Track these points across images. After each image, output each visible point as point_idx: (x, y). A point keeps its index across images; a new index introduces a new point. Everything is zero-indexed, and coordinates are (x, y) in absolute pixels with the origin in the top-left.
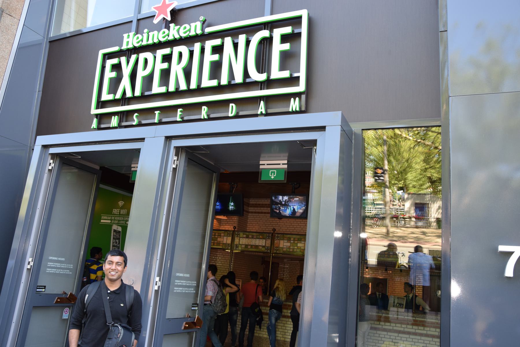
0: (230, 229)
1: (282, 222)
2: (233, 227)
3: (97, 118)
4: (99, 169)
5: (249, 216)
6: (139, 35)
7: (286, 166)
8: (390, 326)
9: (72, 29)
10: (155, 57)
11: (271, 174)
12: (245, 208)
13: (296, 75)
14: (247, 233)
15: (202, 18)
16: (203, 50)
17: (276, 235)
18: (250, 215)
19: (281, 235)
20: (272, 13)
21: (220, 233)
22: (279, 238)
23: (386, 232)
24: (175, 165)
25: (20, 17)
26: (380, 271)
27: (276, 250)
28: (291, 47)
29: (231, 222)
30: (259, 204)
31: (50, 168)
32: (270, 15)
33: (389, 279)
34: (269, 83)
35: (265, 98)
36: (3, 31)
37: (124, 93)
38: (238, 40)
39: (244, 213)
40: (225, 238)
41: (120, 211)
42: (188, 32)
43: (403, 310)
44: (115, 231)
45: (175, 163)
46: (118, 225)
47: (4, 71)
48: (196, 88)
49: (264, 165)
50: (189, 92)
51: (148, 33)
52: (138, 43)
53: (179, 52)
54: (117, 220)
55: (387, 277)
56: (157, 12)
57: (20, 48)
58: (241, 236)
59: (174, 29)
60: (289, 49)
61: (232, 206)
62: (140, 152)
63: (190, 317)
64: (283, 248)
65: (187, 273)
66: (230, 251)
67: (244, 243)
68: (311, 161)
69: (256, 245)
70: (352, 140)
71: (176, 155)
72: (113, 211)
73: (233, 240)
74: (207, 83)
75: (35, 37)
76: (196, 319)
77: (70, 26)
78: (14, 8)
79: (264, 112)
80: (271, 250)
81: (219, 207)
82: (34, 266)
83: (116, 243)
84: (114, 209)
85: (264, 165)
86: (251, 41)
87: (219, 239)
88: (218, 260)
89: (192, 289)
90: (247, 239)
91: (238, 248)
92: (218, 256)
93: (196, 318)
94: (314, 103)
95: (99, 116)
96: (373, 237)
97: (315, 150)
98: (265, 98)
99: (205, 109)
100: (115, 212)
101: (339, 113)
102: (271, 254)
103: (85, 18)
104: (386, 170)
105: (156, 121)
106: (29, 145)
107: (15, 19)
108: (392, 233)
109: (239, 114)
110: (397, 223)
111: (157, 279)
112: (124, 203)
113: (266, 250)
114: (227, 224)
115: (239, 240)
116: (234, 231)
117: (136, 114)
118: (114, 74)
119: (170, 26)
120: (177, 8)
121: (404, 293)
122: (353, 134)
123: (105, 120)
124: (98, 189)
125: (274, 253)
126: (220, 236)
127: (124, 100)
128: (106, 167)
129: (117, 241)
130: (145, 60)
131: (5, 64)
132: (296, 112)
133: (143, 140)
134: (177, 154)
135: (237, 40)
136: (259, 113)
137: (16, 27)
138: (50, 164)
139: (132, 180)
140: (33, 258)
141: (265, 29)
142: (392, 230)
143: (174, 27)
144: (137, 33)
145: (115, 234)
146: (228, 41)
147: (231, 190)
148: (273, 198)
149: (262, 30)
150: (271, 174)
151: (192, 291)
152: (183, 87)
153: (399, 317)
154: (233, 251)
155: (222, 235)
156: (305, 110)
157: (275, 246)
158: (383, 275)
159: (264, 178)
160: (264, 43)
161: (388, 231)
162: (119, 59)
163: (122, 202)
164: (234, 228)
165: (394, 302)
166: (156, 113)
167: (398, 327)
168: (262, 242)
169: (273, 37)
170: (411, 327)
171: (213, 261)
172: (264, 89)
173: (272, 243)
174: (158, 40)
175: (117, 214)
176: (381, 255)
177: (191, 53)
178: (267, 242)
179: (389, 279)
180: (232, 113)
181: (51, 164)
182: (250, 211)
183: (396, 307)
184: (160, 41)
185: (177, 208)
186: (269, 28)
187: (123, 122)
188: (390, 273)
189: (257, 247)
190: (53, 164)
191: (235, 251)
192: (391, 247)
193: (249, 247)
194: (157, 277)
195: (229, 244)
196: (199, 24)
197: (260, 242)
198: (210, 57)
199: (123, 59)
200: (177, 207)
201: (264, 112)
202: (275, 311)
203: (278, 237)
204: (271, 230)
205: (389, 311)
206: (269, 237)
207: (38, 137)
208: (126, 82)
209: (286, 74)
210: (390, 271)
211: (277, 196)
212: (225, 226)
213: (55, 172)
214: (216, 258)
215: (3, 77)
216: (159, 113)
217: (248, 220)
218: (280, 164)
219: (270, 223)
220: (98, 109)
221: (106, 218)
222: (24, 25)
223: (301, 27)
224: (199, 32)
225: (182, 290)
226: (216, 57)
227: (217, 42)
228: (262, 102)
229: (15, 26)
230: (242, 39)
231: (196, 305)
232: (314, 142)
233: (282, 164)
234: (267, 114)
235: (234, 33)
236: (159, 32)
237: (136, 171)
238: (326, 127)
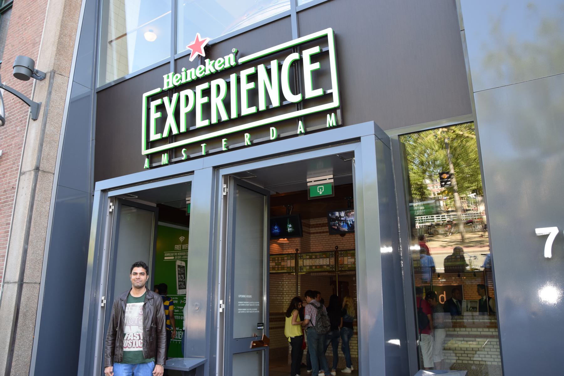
0: (293, 252)
1: (345, 239)
2: (295, 250)
3: (148, 158)
4: (156, 206)
5: (311, 238)
6: (178, 75)
7: (332, 181)
8: (466, 331)
10: (195, 93)
11: (319, 190)
12: (305, 229)
13: (329, 92)
14: (310, 254)
15: (234, 50)
17: (340, 252)
18: (312, 236)
19: (344, 251)
20: (299, 36)
21: (283, 257)
22: (342, 255)
23: (461, 239)
24: (225, 192)
25: (70, 74)
26: (453, 278)
27: (340, 267)
28: (321, 65)
29: (294, 245)
30: (320, 224)
31: (111, 210)
32: (298, 38)
33: (464, 285)
34: (305, 103)
35: (302, 118)
36: (56, 90)
37: (171, 131)
39: (303, 233)
40: (289, 261)
41: (182, 246)
42: (223, 65)
43: (477, 313)
44: (179, 266)
45: (225, 191)
46: (181, 261)
47: (60, 126)
49: (311, 182)
50: (231, 122)
51: (186, 72)
52: (178, 82)
54: (180, 256)
55: (460, 284)
56: (192, 50)
57: (71, 103)
58: (304, 258)
59: (209, 64)
61: (291, 228)
62: (191, 185)
63: (257, 336)
64: (348, 265)
65: (249, 294)
66: (295, 274)
67: (308, 265)
69: (320, 264)
70: (390, 147)
71: (225, 183)
72: (175, 247)
73: (297, 263)
74: (246, 111)
76: (263, 338)
77: (113, 74)
78: (64, 67)
79: (303, 131)
80: (336, 268)
81: (277, 230)
82: (107, 303)
83: (182, 278)
84: (176, 246)
85: (311, 182)
86: (282, 65)
87: (283, 264)
88: (285, 285)
89: (256, 309)
90: (311, 260)
91: (303, 270)
92: (285, 281)
93: (263, 337)
94: (350, 116)
95: (149, 156)
96: (449, 245)
97: (354, 161)
98: (302, 118)
99: (247, 136)
100: (177, 248)
101: (371, 124)
102: (336, 272)
103: (127, 65)
104: (452, 174)
105: (203, 153)
106: (89, 192)
107: (65, 77)
108: (468, 239)
109: (280, 136)
110: (474, 227)
111: (221, 302)
112: (184, 238)
113: (331, 269)
114: (289, 248)
115: (303, 261)
116: (296, 254)
117: (184, 149)
118: (159, 115)
119: (205, 62)
120: (210, 44)
121: (478, 296)
122: (391, 141)
123: (156, 159)
124: (157, 227)
125: (339, 271)
126: (284, 260)
127: (172, 138)
128: (162, 203)
129: (182, 276)
130: (186, 97)
131: (61, 119)
132: (333, 127)
133: (192, 173)
134: (226, 182)
135: (269, 66)
136: (298, 132)
137: (67, 84)
138: (110, 206)
139: (188, 213)
141: (294, 52)
142: (467, 236)
143: (209, 62)
144: (176, 72)
145: (180, 270)
146: (261, 68)
147: (288, 212)
148: (330, 215)
150: (319, 190)
151: (256, 311)
152: (225, 117)
153: (475, 321)
154: (298, 273)
155: (286, 258)
156: (342, 124)
157: (340, 264)
158: (457, 282)
159: (312, 195)
160: (295, 65)
161: (463, 237)
162: (162, 100)
163: (182, 238)
164: (297, 250)
165: (467, 307)
166: (202, 146)
167: (474, 331)
168: (326, 261)
169: (302, 59)
170: (487, 330)
171: (280, 287)
172: (300, 110)
173: (336, 261)
174: (195, 76)
175: (179, 249)
176: (447, 260)
177: (228, 84)
178: (331, 260)
179: (464, 285)
180: (273, 136)
181: (111, 207)
182: (311, 232)
183: (470, 311)
184: (198, 78)
185: (232, 233)
186: (298, 51)
187: (173, 159)
188: (464, 279)
189: (321, 266)
190: (113, 207)
191: (299, 274)
192: (458, 250)
193: (314, 268)
194: (221, 300)
195: (293, 267)
196: (232, 56)
197: (324, 261)
198: (246, 86)
199: (166, 99)
200: (231, 232)
201: (303, 131)
202: (346, 328)
203: (341, 254)
204: (334, 248)
205: (463, 316)
206: (332, 255)
207: (96, 183)
208: (171, 121)
209: (319, 92)
210: (463, 277)
211: (334, 212)
212: (288, 250)
213: (116, 214)
214: (282, 283)
215: (59, 132)
216: (205, 146)
217: (311, 242)
218: (326, 179)
219: (333, 242)
220: (148, 149)
221: (169, 254)
223: (328, 46)
224: (233, 63)
225: (245, 311)
226: (252, 85)
227: (251, 70)
228: (300, 122)
229: (65, 83)
230: (274, 64)
231: (262, 325)
232: (351, 154)
233: (328, 178)
234: (306, 133)
235: (265, 60)
236: (196, 68)
237: (190, 204)
238: (361, 138)
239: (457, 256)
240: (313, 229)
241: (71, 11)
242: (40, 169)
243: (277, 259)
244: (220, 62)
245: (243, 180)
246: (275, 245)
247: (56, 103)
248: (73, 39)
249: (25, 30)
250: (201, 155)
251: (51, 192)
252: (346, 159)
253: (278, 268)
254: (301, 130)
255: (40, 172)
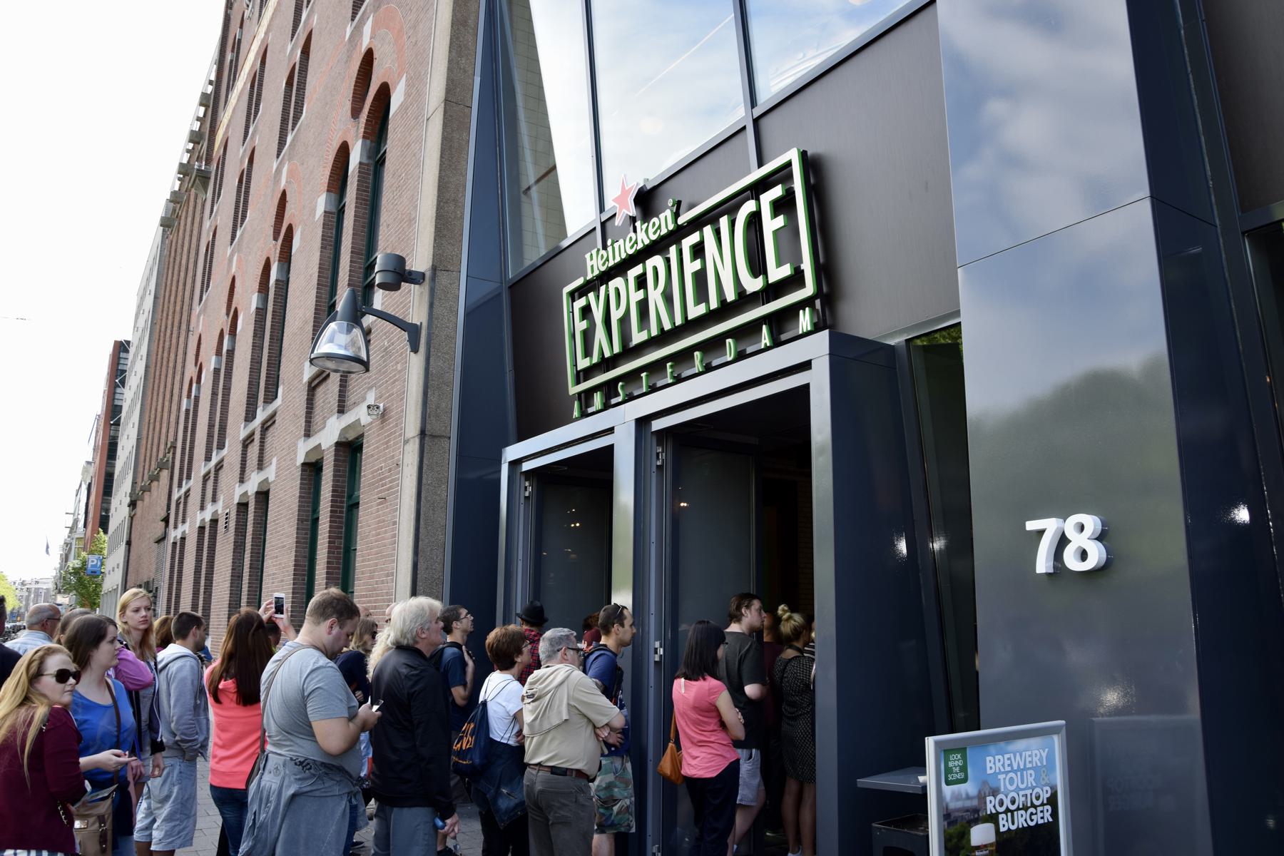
9: (543, 252)
16: (680, 252)
36: (440, 299)
56: (617, 206)
57: (467, 315)
75: (487, 288)
95: (583, 395)
105: (670, 381)
133: (610, 430)
137: (457, 284)
138: (526, 487)
140: (661, 640)
177: (668, 261)
181: (528, 489)
209: (786, 271)
213: (533, 501)
222: (467, 276)
228: (764, 327)
241: (452, 158)
242: (427, 433)
244: (654, 224)
247: (442, 320)
248: (460, 204)
249: (400, 197)
250: (796, 335)
251: (447, 469)
254: (765, 341)
255: (427, 439)
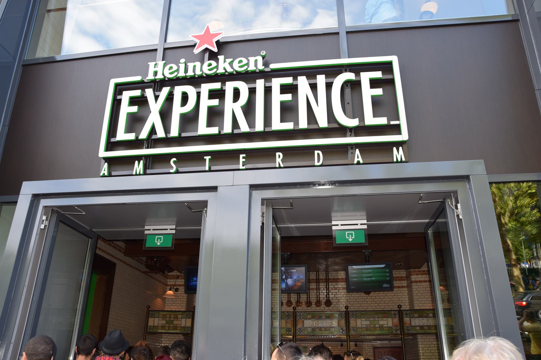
9: (46, 55)
11: (157, 240)
22: (408, 316)
28: (139, 109)
37: (153, 131)
38: (298, 82)
40: (183, 320)
48: (135, 139)
53: (182, 92)
60: (136, 111)
68: (201, 227)
74: (277, 125)
87: (175, 322)
97: (205, 212)
126: (177, 318)
149: (342, 73)
150: (157, 240)
155: (180, 316)
159: (149, 244)
166: (205, 160)
172: (151, 148)
204: (344, 308)
233: (170, 229)
239: (376, 325)
240: (398, 282)
243: (168, 316)
245: (66, 215)
246: (159, 299)
252: (193, 210)
253: (169, 327)
254: (104, 172)
